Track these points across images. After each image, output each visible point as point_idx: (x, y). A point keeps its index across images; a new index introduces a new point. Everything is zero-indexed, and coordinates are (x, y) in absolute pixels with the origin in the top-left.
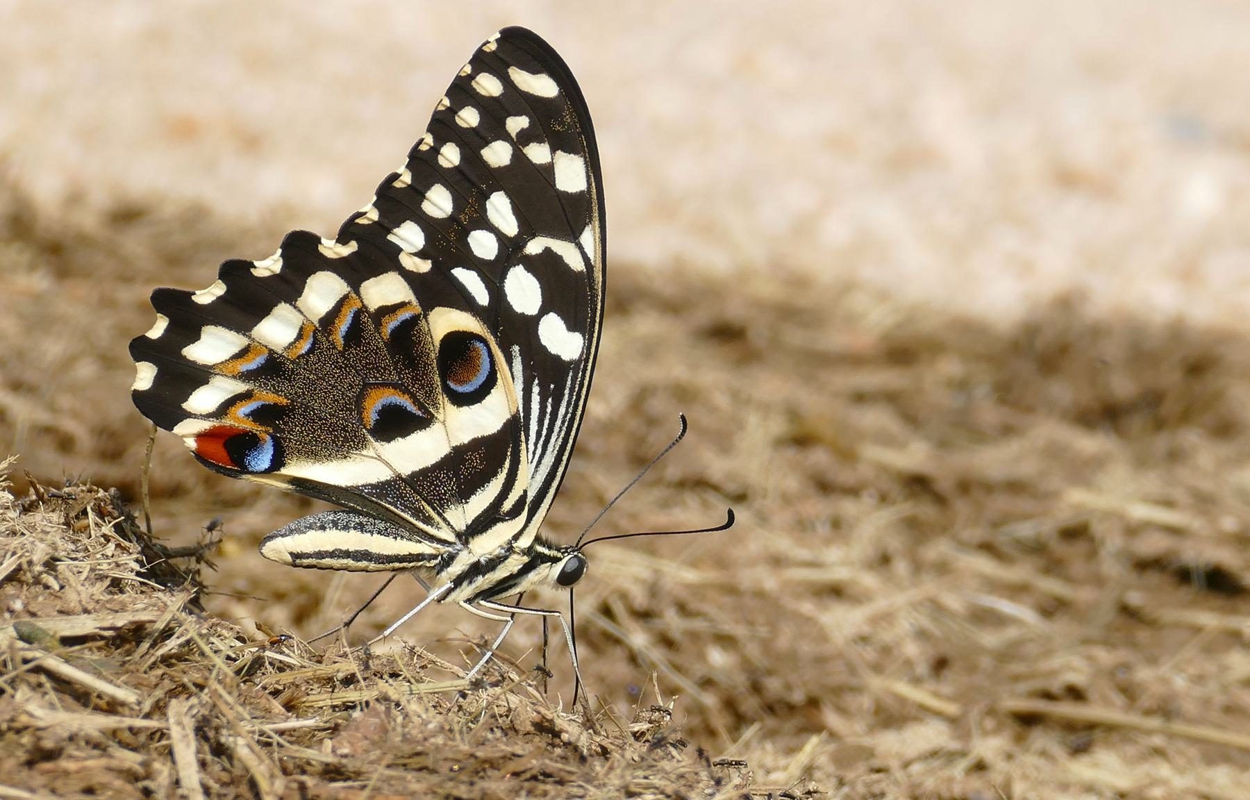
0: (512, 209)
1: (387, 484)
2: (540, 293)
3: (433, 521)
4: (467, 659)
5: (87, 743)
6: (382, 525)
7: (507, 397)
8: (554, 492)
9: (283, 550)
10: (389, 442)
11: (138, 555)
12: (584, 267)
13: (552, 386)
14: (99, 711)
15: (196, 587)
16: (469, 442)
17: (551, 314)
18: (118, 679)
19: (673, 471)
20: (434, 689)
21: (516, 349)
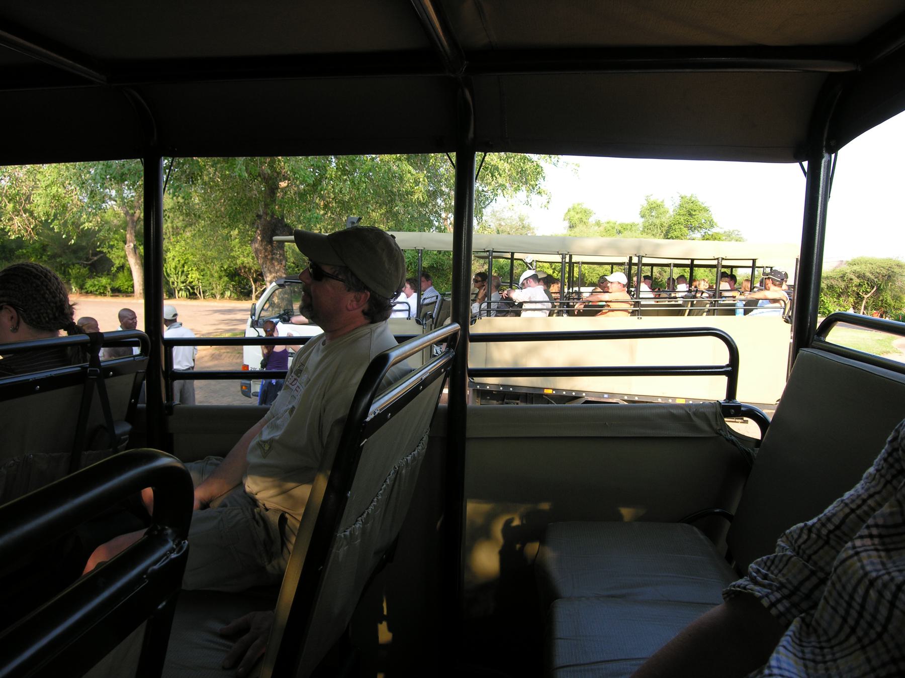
0: (562, 155)
1: (397, 294)
2: (746, 435)
3: (437, 230)
4: (797, 528)
5: (889, 352)
6: (24, 266)
7: (427, 17)
8: (681, 436)
9: (424, 293)
10: (261, 363)
11: (216, 351)
12: (61, 336)
13: (384, 634)
14: (192, 300)
15: (314, 319)
16: (782, 397)
17: (727, 378)
18: (252, 299)
19: (688, 237)
20: (735, 422)
21: (147, 536)
